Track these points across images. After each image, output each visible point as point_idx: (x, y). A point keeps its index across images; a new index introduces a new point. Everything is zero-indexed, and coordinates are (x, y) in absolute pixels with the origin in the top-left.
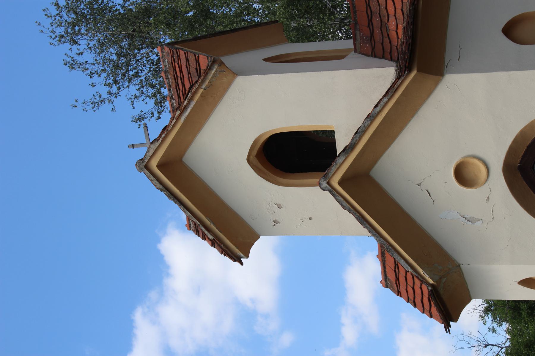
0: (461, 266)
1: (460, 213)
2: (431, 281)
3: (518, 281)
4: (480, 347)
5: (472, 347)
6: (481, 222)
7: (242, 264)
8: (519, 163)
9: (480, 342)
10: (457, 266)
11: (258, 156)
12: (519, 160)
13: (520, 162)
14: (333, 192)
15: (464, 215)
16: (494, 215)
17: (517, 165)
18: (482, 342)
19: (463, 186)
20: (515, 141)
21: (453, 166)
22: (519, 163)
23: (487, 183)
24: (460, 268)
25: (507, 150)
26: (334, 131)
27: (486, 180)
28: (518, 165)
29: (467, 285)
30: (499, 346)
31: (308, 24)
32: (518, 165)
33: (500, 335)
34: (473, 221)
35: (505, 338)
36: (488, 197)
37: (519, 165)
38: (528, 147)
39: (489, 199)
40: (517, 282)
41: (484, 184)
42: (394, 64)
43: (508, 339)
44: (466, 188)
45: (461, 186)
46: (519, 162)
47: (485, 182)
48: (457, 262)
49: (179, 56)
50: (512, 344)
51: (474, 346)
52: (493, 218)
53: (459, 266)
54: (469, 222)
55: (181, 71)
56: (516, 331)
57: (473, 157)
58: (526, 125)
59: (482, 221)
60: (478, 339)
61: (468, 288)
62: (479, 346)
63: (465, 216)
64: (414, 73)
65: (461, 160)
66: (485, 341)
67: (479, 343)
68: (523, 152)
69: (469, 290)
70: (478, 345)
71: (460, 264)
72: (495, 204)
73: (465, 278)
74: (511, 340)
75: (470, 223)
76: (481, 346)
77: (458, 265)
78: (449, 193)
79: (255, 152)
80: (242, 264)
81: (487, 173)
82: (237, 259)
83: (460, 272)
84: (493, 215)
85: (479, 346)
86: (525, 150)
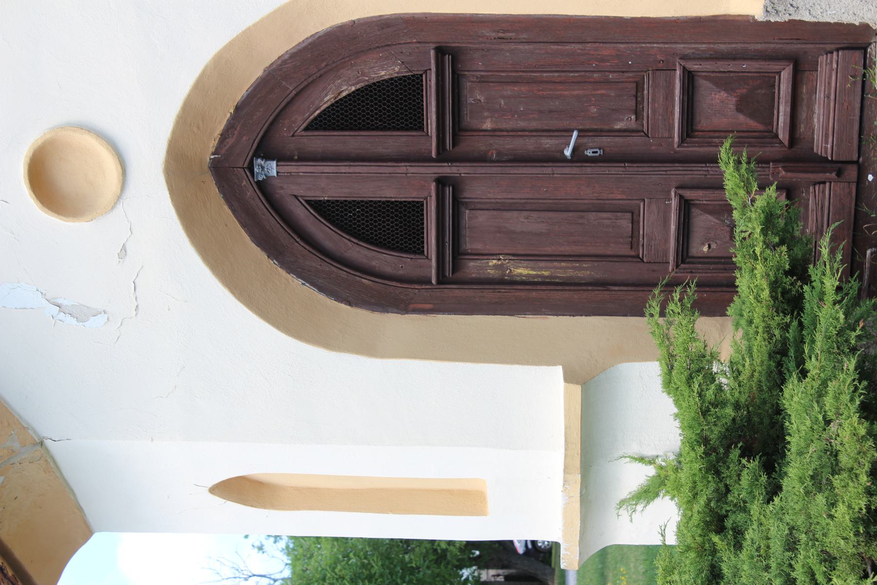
0: (48, 443)
1: (44, 292)
3: (210, 485)
4: (238, 579)
5: (223, 579)
6: (102, 318)
8: (213, 154)
9: (237, 570)
10: (35, 444)
12: (213, 144)
13: (216, 149)
15: (53, 299)
16: (138, 299)
17: (208, 160)
18: (242, 571)
19: (53, 214)
20: (201, 87)
21: (25, 154)
22: (213, 154)
23: (120, 207)
24: (47, 450)
25: (178, 112)
27: (119, 198)
28: (210, 159)
29: (74, 494)
30: (270, 578)
31: (249, 192)
32: (208, 157)
33: (273, 557)
34: (81, 314)
35: (282, 562)
36: (124, 245)
37: (212, 157)
38: (237, 109)
39: (126, 252)
40: (207, 489)
41: (113, 208)
43: (287, 564)
44: (61, 217)
45: (46, 213)
46: (212, 150)
47: (116, 203)
48: (35, 431)
50: (293, 573)
51: (227, 579)
52: (137, 306)
53: (42, 443)
54: (69, 319)
56: (301, 551)
57: (82, 129)
58: (232, 38)
59: (106, 315)
60: (235, 566)
61: (78, 503)
62: (235, 578)
63: (59, 301)
65: (48, 136)
66: (246, 568)
67: (236, 572)
68: (225, 122)
69: (80, 509)
70: (233, 576)
71: (44, 438)
72: (143, 267)
73: (65, 475)
74: (293, 566)
75: (74, 321)
76: (240, 578)
77: (38, 441)
78: (13, 234)
81: (121, 178)
83: (46, 461)
84: (136, 298)
85: (235, 578)
86: (229, 115)
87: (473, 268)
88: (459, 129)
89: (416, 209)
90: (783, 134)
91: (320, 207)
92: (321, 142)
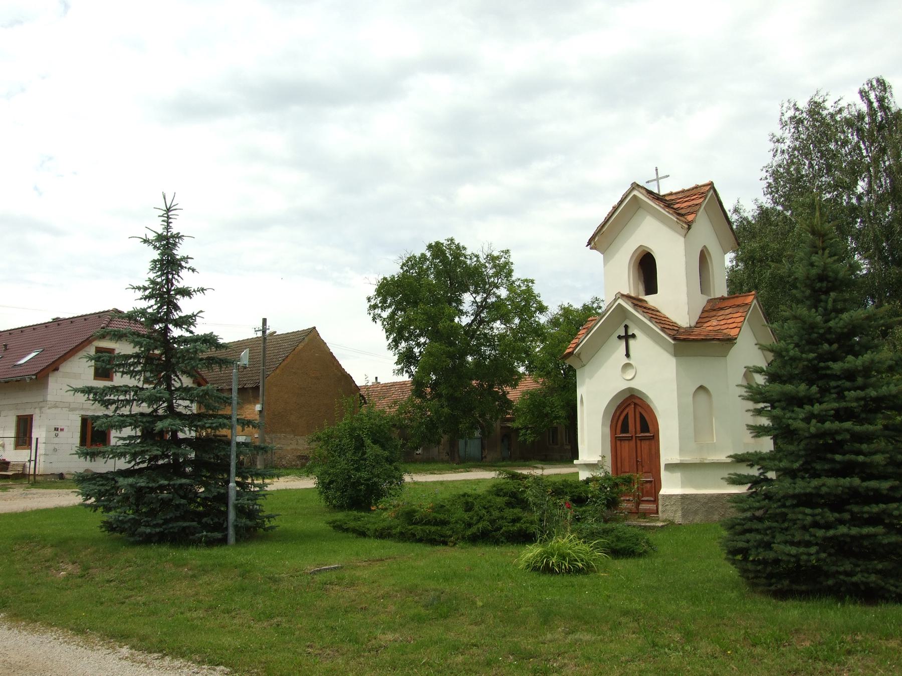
2: (575, 352)
7: (587, 246)
11: (644, 250)
14: (615, 300)
20: (643, 393)
26: (656, 292)
42: (693, 324)
49: (701, 198)
55: (693, 200)
64: (673, 342)
79: (646, 250)
80: (587, 246)
82: (589, 243)
87: (618, 443)
88: (641, 440)
89: (648, 431)
90: (643, 499)
91: (627, 414)
92: (625, 413)
